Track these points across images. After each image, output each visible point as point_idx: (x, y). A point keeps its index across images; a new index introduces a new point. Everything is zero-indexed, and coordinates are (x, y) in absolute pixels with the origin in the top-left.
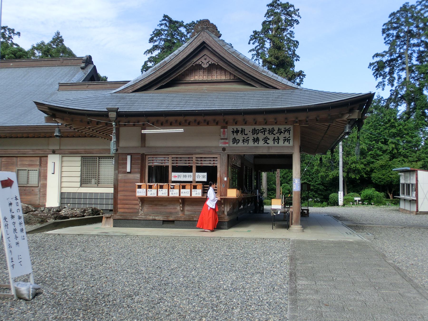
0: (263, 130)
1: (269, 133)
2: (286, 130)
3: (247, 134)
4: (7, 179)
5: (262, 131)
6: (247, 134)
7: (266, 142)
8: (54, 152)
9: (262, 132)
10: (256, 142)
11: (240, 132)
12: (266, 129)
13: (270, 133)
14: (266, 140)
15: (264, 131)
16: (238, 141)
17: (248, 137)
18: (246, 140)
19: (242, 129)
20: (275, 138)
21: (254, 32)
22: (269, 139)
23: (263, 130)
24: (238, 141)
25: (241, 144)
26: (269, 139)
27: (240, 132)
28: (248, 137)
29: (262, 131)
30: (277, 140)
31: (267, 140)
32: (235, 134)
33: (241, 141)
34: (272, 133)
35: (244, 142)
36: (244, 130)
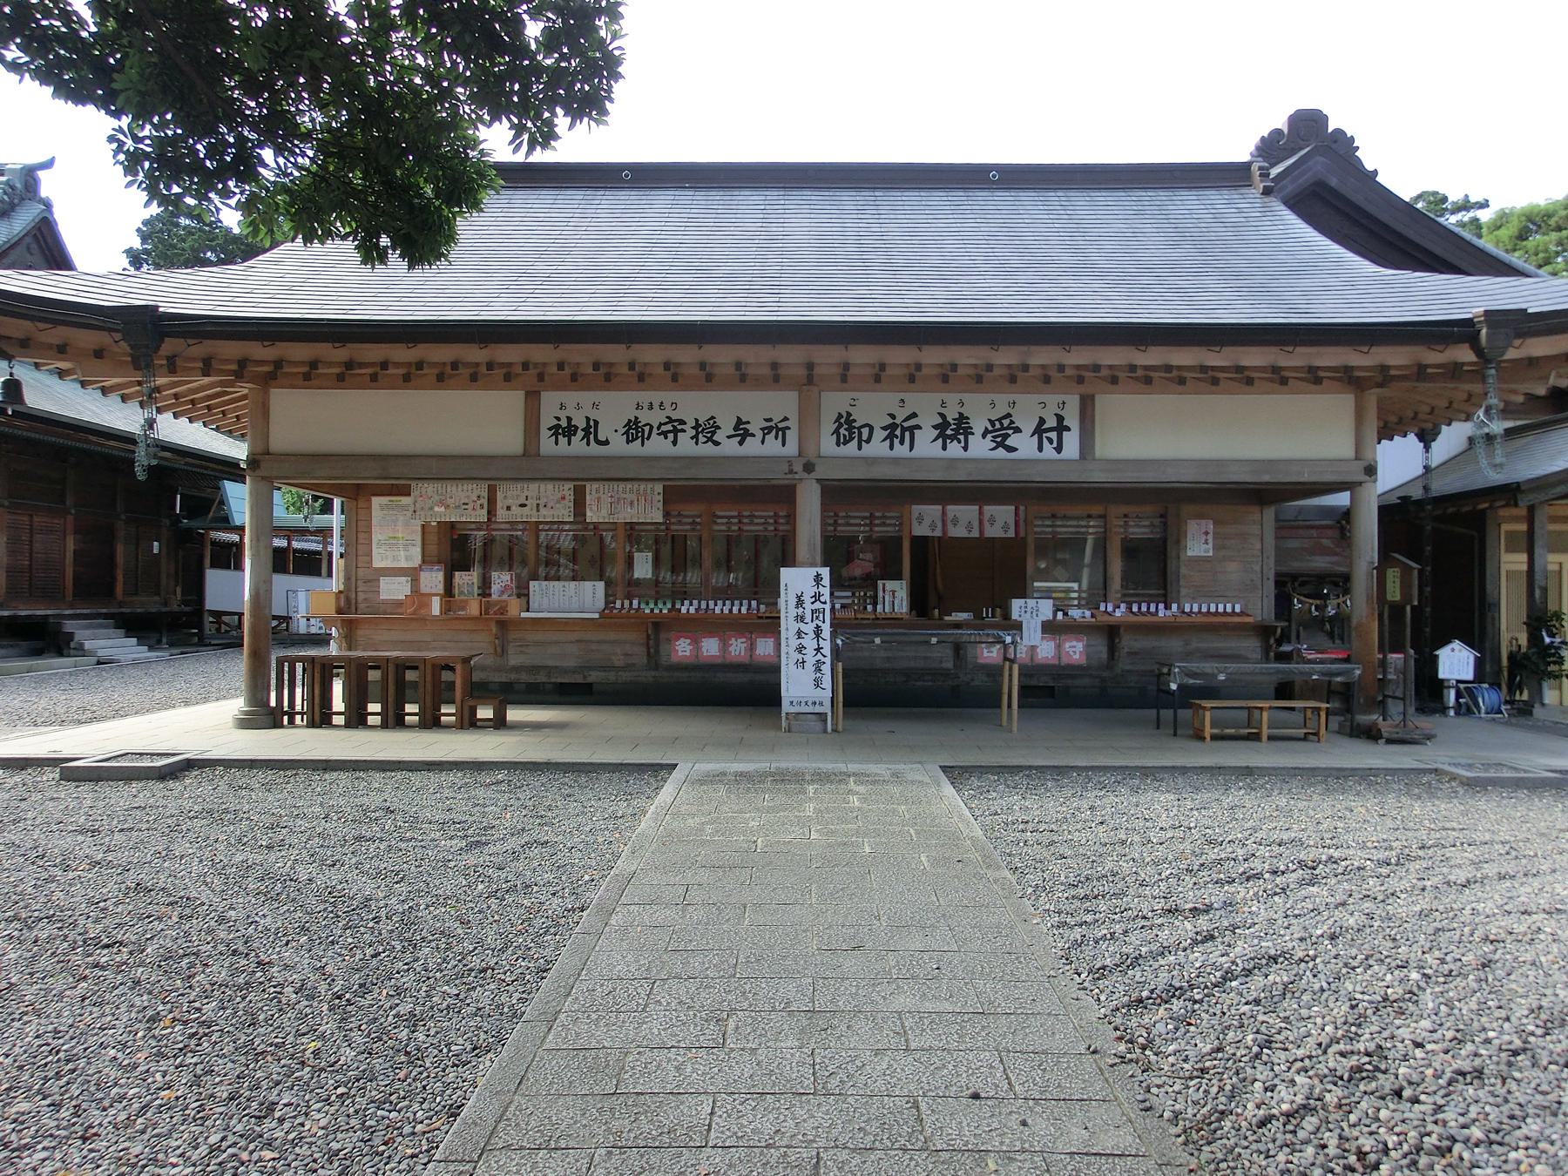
0: (669, 427)
1: (695, 437)
2: (770, 429)
3: (606, 443)
4: (925, 347)
5: (664, 428)
6: (606, 443)
7: (999, 445)
8: (399, 604)
9: (665, 434)
10: (953, 438)
11: (580, 434)
12: (682, 422)
13: (702, 439)
14: (1001, 431)
15: (675, 431)
16: (865, 431)
17: (914, 415)
18: (904, 430)
19: (588, 419)
20: (1042, 421)
21: (606, 123)
22: (1017, 430)
23: (669, 427)
24: (865, 431)
25: (878, 447)
26: (1017, 430)
27: (580, 434)
28: (914, 415)
29: (664, 428)
30: (1053, 435)
31: (1007, 436)
32: (563, 440)
33: (879, 434)
34: (710, 439)
35: (891, 437)
36: (596, 423)
